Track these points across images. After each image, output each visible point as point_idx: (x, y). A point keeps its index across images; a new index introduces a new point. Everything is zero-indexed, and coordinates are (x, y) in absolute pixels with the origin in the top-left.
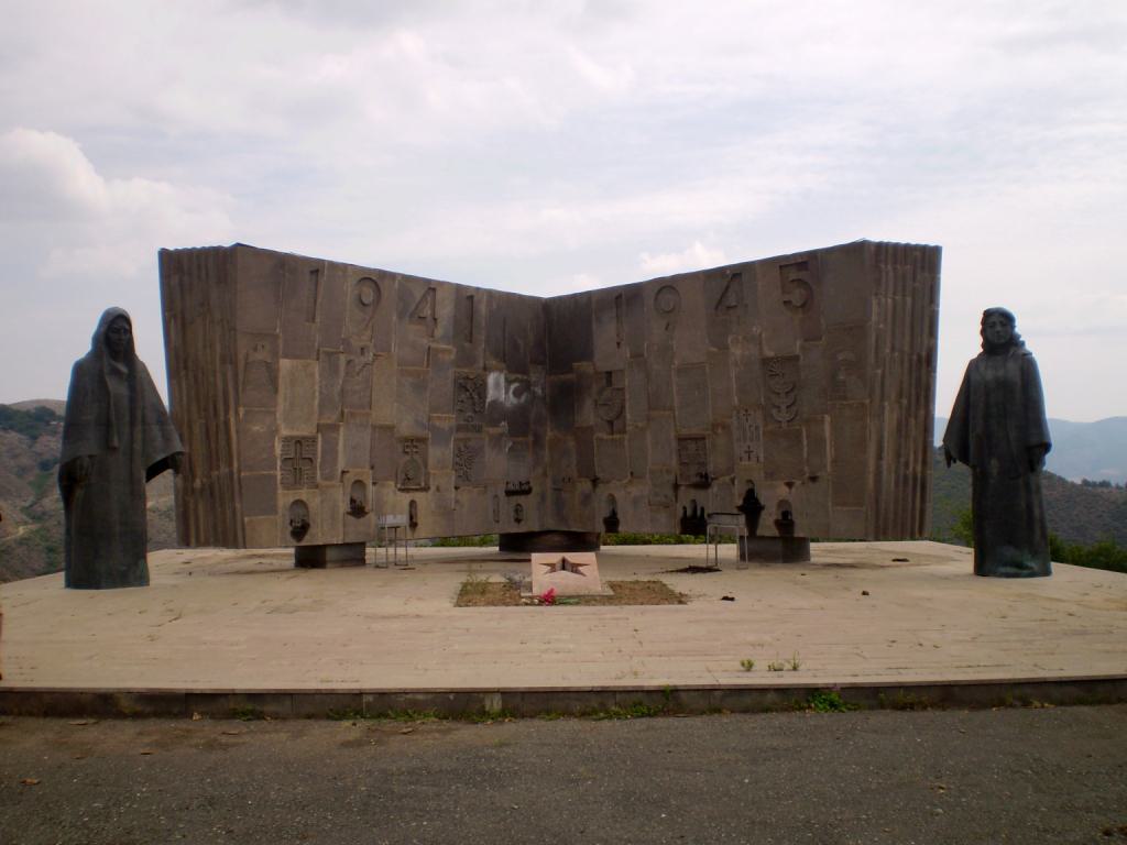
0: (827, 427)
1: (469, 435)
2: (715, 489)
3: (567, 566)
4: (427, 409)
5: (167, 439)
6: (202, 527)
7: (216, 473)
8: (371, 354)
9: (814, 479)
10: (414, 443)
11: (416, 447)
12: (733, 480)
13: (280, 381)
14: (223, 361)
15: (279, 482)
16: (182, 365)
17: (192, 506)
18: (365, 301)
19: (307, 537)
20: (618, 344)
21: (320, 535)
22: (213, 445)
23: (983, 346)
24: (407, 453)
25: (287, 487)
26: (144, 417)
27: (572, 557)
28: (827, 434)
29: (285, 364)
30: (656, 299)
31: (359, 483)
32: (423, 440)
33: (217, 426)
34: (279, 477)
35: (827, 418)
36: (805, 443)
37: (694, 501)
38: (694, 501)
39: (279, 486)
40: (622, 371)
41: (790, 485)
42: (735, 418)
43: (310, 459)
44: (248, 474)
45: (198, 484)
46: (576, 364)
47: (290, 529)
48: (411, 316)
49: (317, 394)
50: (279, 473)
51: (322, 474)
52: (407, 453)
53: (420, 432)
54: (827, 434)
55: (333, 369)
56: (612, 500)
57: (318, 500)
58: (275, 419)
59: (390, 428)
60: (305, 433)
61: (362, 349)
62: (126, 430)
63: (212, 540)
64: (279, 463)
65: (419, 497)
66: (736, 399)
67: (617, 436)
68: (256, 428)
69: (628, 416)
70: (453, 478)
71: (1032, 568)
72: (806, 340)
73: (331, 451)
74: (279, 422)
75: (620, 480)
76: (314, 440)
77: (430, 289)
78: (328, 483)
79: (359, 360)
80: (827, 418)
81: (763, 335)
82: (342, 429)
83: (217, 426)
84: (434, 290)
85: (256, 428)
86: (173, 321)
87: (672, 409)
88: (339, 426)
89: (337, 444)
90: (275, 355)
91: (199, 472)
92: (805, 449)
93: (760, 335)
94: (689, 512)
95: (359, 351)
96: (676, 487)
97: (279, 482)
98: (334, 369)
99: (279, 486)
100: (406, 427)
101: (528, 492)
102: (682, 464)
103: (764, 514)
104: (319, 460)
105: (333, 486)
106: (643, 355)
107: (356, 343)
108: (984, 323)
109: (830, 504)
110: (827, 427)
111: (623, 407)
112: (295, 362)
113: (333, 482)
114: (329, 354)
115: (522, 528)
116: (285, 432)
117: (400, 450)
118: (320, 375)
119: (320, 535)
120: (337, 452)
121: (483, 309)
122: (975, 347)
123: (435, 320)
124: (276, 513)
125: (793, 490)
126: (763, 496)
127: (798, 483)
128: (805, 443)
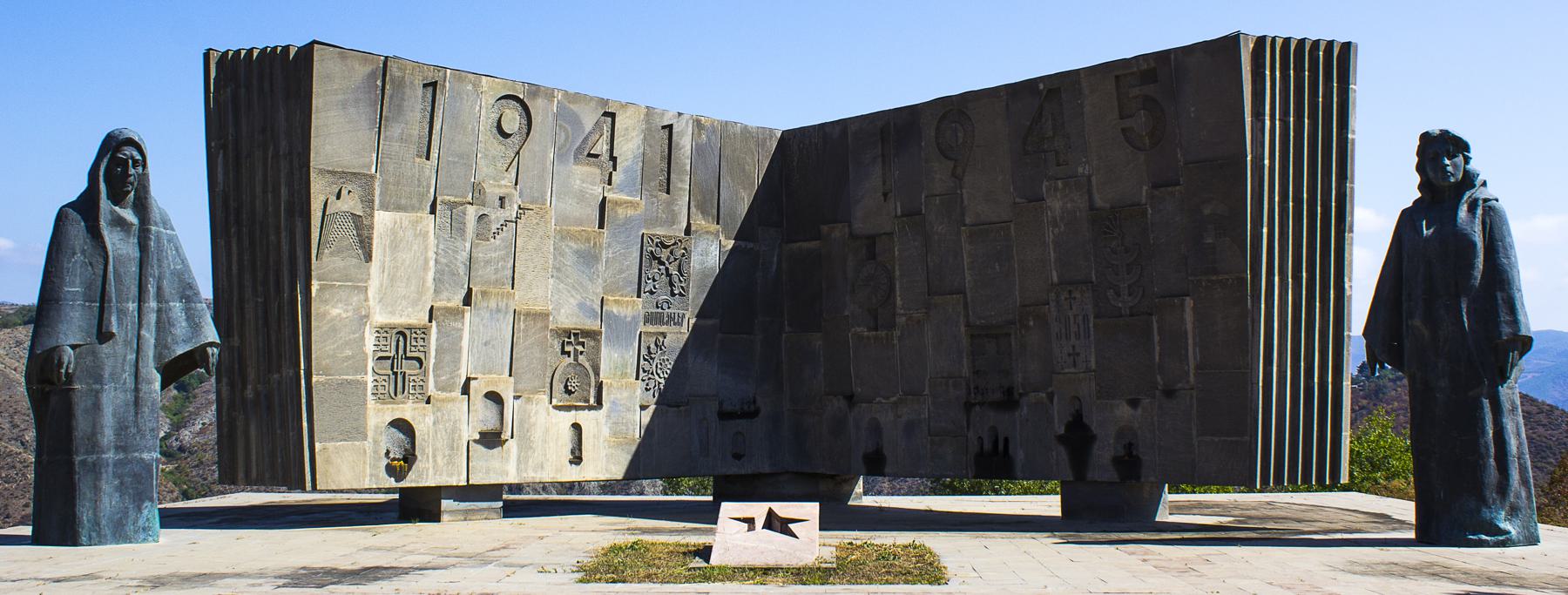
0: (1189, 316)
1: (663, 329)
2: (1025, 410)
3: (777, 524)
4: (600, 290)
5: (195, 326)
6: (254, 458)
7: (276, 376)
8: (516, 207)
9: (1169, 393)
10: (576, 340)
11: (583, 344)
12: (1051, 397)
13: (375, 242)
14: (290, 212)
15: (369, 392)
16: (232, 218)
17: (240, 424)
18: (507, 128)
19: (411, 476)
20: (885, 195)
21: (431, 471)
22: (273, 339)
23: (1421, 187)
24: (568, 354)
25: (379, 397)
26: (159, 288)
27: (784, 509)
28: (1189, 327)
29: (383, 220)
30: (938, 129)
31: (495, 398)
32: (593, 335)
33: (280, 308)
34: (370, 385)
35: (1189, 302)
36: (1156, 338)
37: (994, 429)
38: (994, 429)
39: (370, 397)
40: (890, 234)
41: (1134, 403)
42: (1052, 304)
43: (419, 360)
44: (322, 378)
45: (249, 393)
46: (825, 228)
47: (385, 462)
48: (579, 150)
49: (432, 263)
50: (370, 378)
51: (436, 382)
52: (568, 354)
53: (592, 324)
54: (1189, 327)
55: (457, 227)
56: (876, 429)
57: (430, 420)
58: (366, 300)
59: (544, 316)
60: (413, 321)
61: (502, 199)
62: (132, 306)
63: (267, 475)
64: (370, 364)
65: (584, 418)
66: (1055, 274)
67: (882, 333)
68: (335, 312)
69: (899, 302)
70: (639, 392)
71: (1509, 533)
72: (1155, 186)
73: (450, 349)
74: (371, 303)
75: (888, 398)
76: (425, 331)
77: (606, 114)
78: (444, 395)
79: (497, 216)
80: (1189, 302)
81: (1094, 179)
82: (467, 315)
83: (280, 308)
84: (613, 115)
85: (335, 312)
86: (221, 152)
87: (962, 292)
88: (463, 312)
89: (461, 338)
90: (368, 202)
91: (252, 374)
92: (1157, 348)
93: (1089, 178)
94: (987, 446)
95: (498, 203)
96: (968, 407)
97: (369, 392)
98: (457, 227)
99: (370, 397)
100: (568, 317)
101: (754, 414)
102: (976, 373)
103: (1096, 450)
104: (432, 361)
105: (453, 400)
106: (919, 213)
107: (493, 191)
108: (1421, 152)
109: (1194, 432)
110: (1189, 316)
111: (892, 288)
112: (398, 215)
113: (453, 394)
114: (452, 206)
115: (746, 469)
116: (380, 318)
117: (558, 349)
118: (437, 237)
119: (431, 471)
120: (460, 351)
121: (685, 143)
122: (1408, 191)
123: (613, 159)
124: (365, 438)
125: (1140, 411)
126: (1094, 421)
127: (1146, 401)
128: (1156, 338)
